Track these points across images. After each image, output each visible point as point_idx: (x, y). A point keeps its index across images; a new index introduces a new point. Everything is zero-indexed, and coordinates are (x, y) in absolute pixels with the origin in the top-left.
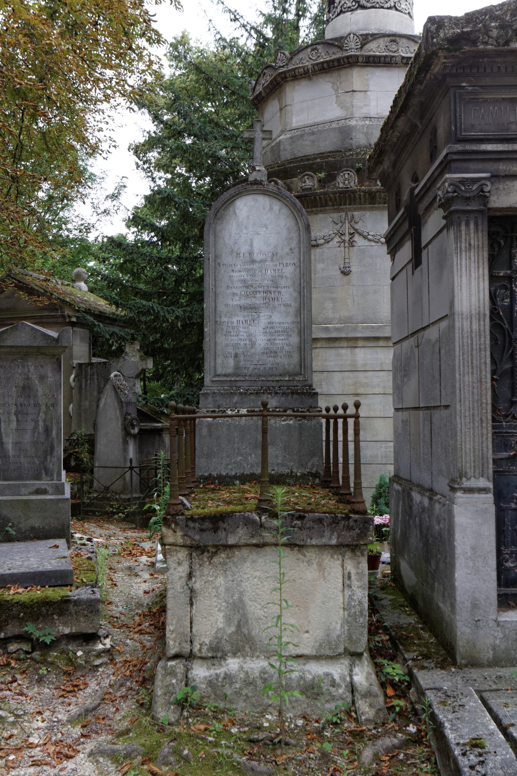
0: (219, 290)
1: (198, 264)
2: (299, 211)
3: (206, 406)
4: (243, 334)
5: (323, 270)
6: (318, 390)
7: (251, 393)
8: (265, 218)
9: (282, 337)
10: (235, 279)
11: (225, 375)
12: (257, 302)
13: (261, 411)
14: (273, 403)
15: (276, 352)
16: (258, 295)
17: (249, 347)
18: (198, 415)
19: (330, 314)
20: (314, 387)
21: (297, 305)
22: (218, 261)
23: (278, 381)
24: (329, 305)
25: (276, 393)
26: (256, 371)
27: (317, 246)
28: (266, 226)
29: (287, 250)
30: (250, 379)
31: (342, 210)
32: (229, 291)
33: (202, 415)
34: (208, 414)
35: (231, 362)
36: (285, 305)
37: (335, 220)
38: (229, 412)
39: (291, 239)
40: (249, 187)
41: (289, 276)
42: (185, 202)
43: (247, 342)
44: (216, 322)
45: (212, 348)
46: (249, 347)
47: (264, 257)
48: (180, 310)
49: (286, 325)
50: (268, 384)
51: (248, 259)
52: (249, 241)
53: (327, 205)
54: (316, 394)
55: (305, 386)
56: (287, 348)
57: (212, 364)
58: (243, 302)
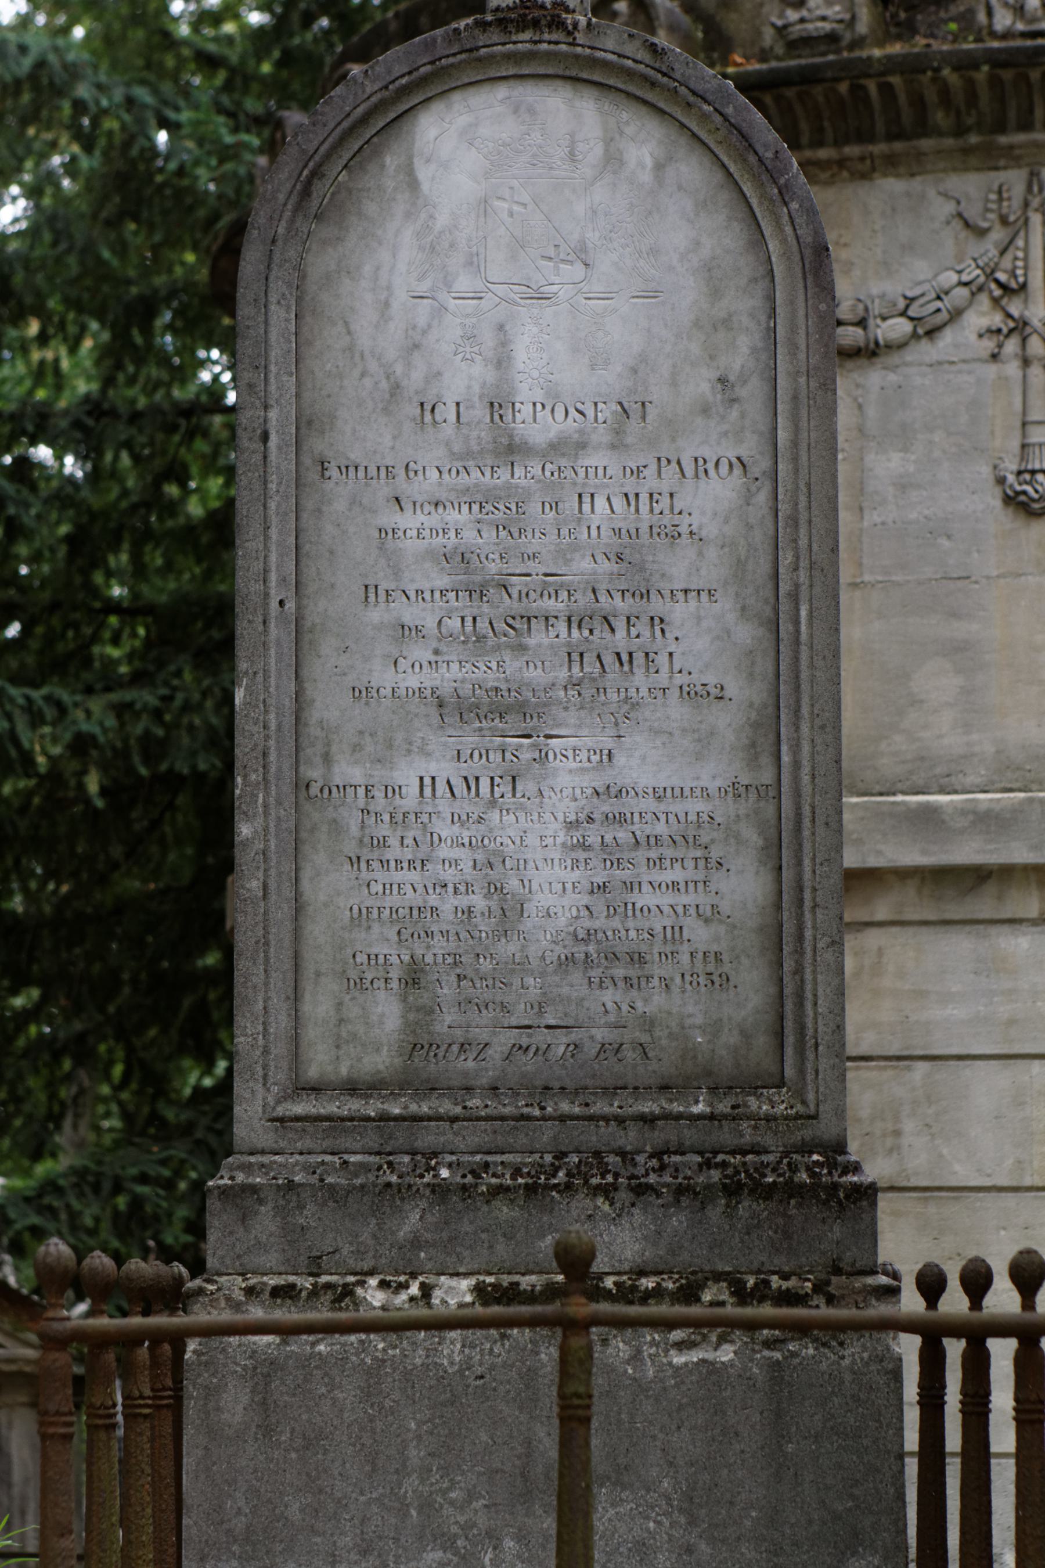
0: (317, 609)
1: (201, 446)
2: (768, 172)
3: (242, 1264)
4: (453, 858)
5: (903, 485)
6: (875, 1170)
7: (499, 1190)
8: (580, 208)
9: (675, 874)
10: (411, 545)
11: (352, 1088)
12: (534, 674)
13: (551, 1293)
14: (621, 1243)
15: (638, 959)
16: (538, 637)
17: (484, 926)
18: (201, 1315)
19: (944, 734)
20: (854, 1150)
21: (758, 693)
22: (317, 445)
23: (648, 1120)
24: (937, 683)
25: (640, 1190)
26: (528, 1063)
27: (870, 352)
28: (582, 255)
29: (700, 384)
30: (495, 1107)
31: (1012, 157)
32: (376, 615)
33: (225, 1316)
34: (257, 1313)
35: (386, 1013)
36: (689, 694)
37: (972, 212)
38: (374, 1296)
39: (727, 323)
40: (493, 43)
41: (711, 530)
42: (130, 102)
43: (478, 901)
44: (301, 786)
45: (281, 933)
46: (484, 926)
47: (572, 425)
48: (96, 705)
49: (696, 806)
50: (596, 1136)
51: (481, 434)
52: (488, 339)
53: (923, 128)
54: (868, 1193)
55: (806, 1149)
56: (699, 935)
57: (281, 1022)
58: (452, 675)
